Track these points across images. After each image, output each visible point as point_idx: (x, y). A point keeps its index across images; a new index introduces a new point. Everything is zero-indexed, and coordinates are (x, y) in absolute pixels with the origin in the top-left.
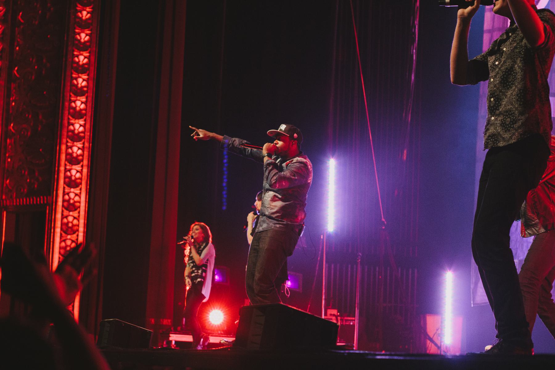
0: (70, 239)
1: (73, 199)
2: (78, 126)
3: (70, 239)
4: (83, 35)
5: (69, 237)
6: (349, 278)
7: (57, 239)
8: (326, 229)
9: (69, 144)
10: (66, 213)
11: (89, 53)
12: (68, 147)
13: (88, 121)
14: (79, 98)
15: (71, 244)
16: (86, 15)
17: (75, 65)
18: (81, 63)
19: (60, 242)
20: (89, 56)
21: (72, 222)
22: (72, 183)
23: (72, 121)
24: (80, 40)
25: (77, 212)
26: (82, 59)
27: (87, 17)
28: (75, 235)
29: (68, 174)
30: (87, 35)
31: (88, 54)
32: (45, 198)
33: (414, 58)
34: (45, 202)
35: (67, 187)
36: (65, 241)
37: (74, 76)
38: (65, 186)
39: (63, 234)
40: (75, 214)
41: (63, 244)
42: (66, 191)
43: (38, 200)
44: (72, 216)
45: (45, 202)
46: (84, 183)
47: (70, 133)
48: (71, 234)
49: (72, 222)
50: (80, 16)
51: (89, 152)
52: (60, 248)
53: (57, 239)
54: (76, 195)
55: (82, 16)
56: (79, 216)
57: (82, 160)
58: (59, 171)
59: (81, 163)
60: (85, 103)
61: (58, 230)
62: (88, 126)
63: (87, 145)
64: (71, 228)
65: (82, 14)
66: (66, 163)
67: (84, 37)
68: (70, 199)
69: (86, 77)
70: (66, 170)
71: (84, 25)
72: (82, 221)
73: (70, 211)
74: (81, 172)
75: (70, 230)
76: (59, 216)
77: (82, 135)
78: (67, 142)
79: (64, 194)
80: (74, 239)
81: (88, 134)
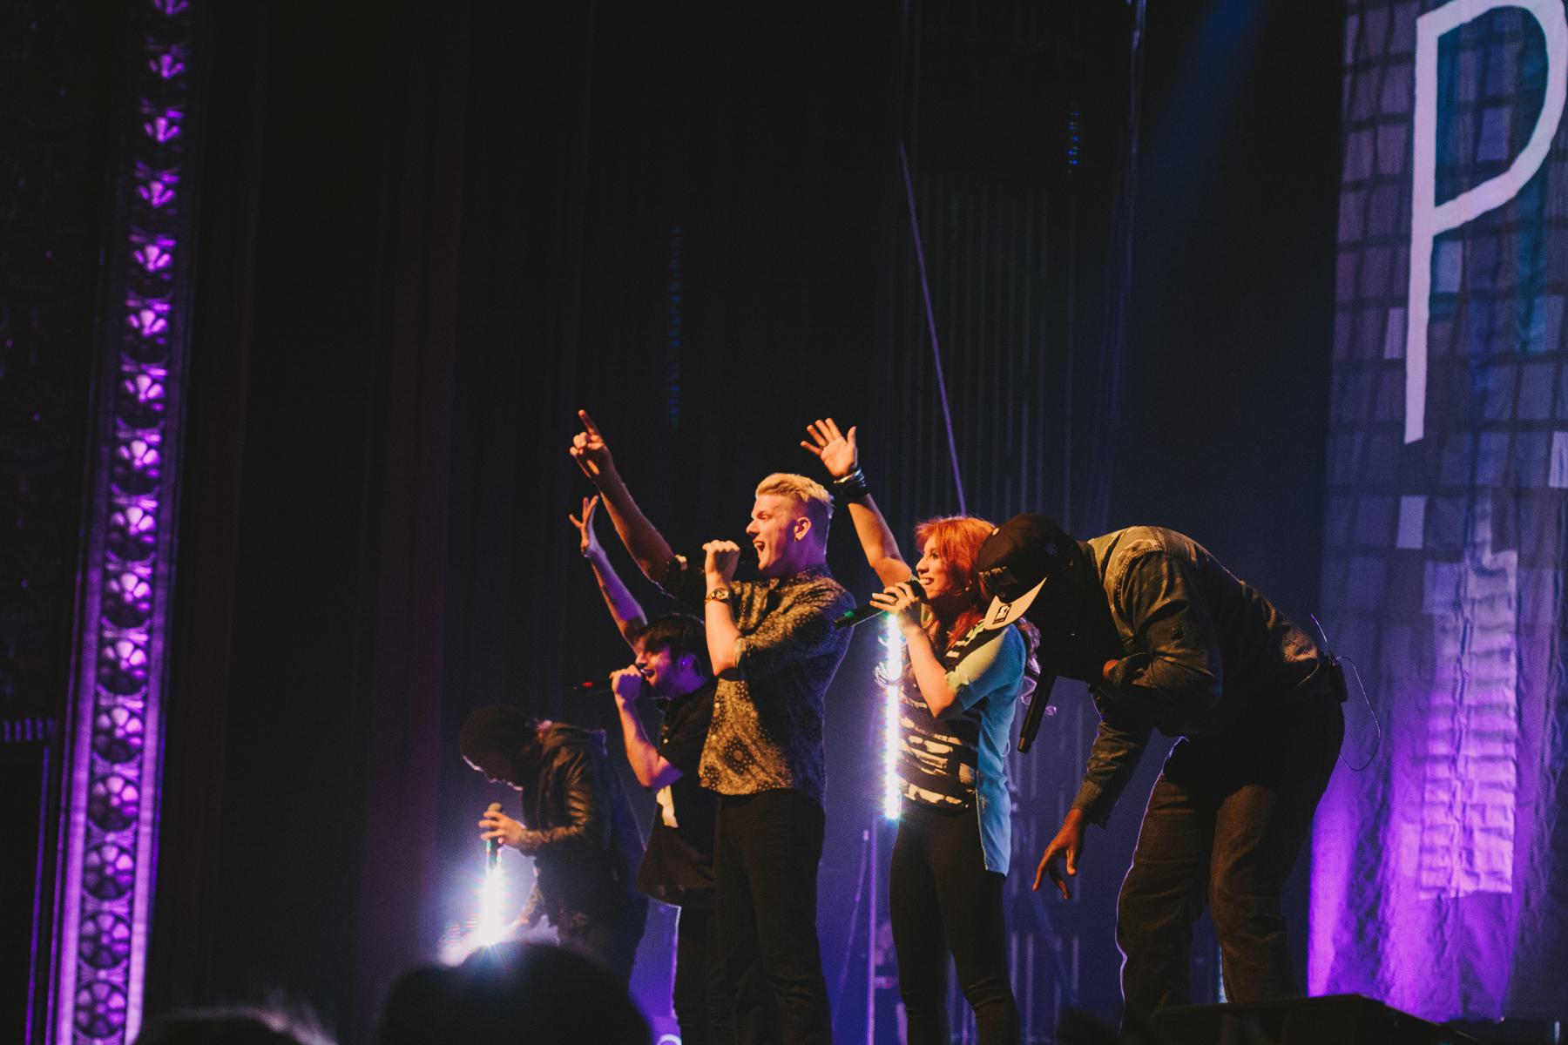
0: (114, 844)
1: (123, 727)
2: (126, 715)
3: (114, 844)
4: (148, 317)
5: (111, 837)
6: (1024, 496)
7: (78, 845)
8: (881, 813)
9: (111, 567)
10: (101, 767)
11: (157, 499)
12: (98, 711)
13: (153, 700)
14: (117, 768)
15: (113, 927)
16: (160, 256)
17: (130, 338)
18: (146, 331)
19: (86, 853)
20: (170, 311)
21: (119, 795)
22: (110, 816)
23: (122, 501)
24: (147, 203)
25: (119, 970)
26: (150, 321)
27: (161, 263)
28: (128, 833)
29: (105, 721)
30: (154, 381)
31: (165, 307)
32: (39, 725)
33: (1135, 43)
34: (40, 736)
35: (104, 693)
36: (98, 849)
37: (126, 368)
38: (91, 824)
39: (95, 830)
40: (125, 839)
41: (90, 927)
42: (104, 702)
43: (18, 728)
44: (124, 707)
45: (40, 736)
46: (153, 680)
47: (115, 536)
48: (116, 830)
49: (119, 795)
50: (145, 195)
51: (156, 786)
52: (86, 869)
53: (78, 845)
54: (118, 919)
55: (151, 197)
56: (140, 777)
57: (145, 682)
58: (71, 786)
59: (148, 623)
60: (146, 648)
61: (75, 891)
62: (166, 515)
63: (163, 568)
64: (112, 879)
65: (149, 191)
66: (104, 621)
67: (142, 453)
68: (114, 725)
69: (141, 638)
70: (93, 779)
71: (148, 351)
72: (140, 928)
73: (114, 763)
74: (132, 852)
75: (105, 954)
76: (83, 776)
77: (137, 741)
78: (101, 628)
79: (85, 917)
80: (125, 843)
81: (168, 537)
